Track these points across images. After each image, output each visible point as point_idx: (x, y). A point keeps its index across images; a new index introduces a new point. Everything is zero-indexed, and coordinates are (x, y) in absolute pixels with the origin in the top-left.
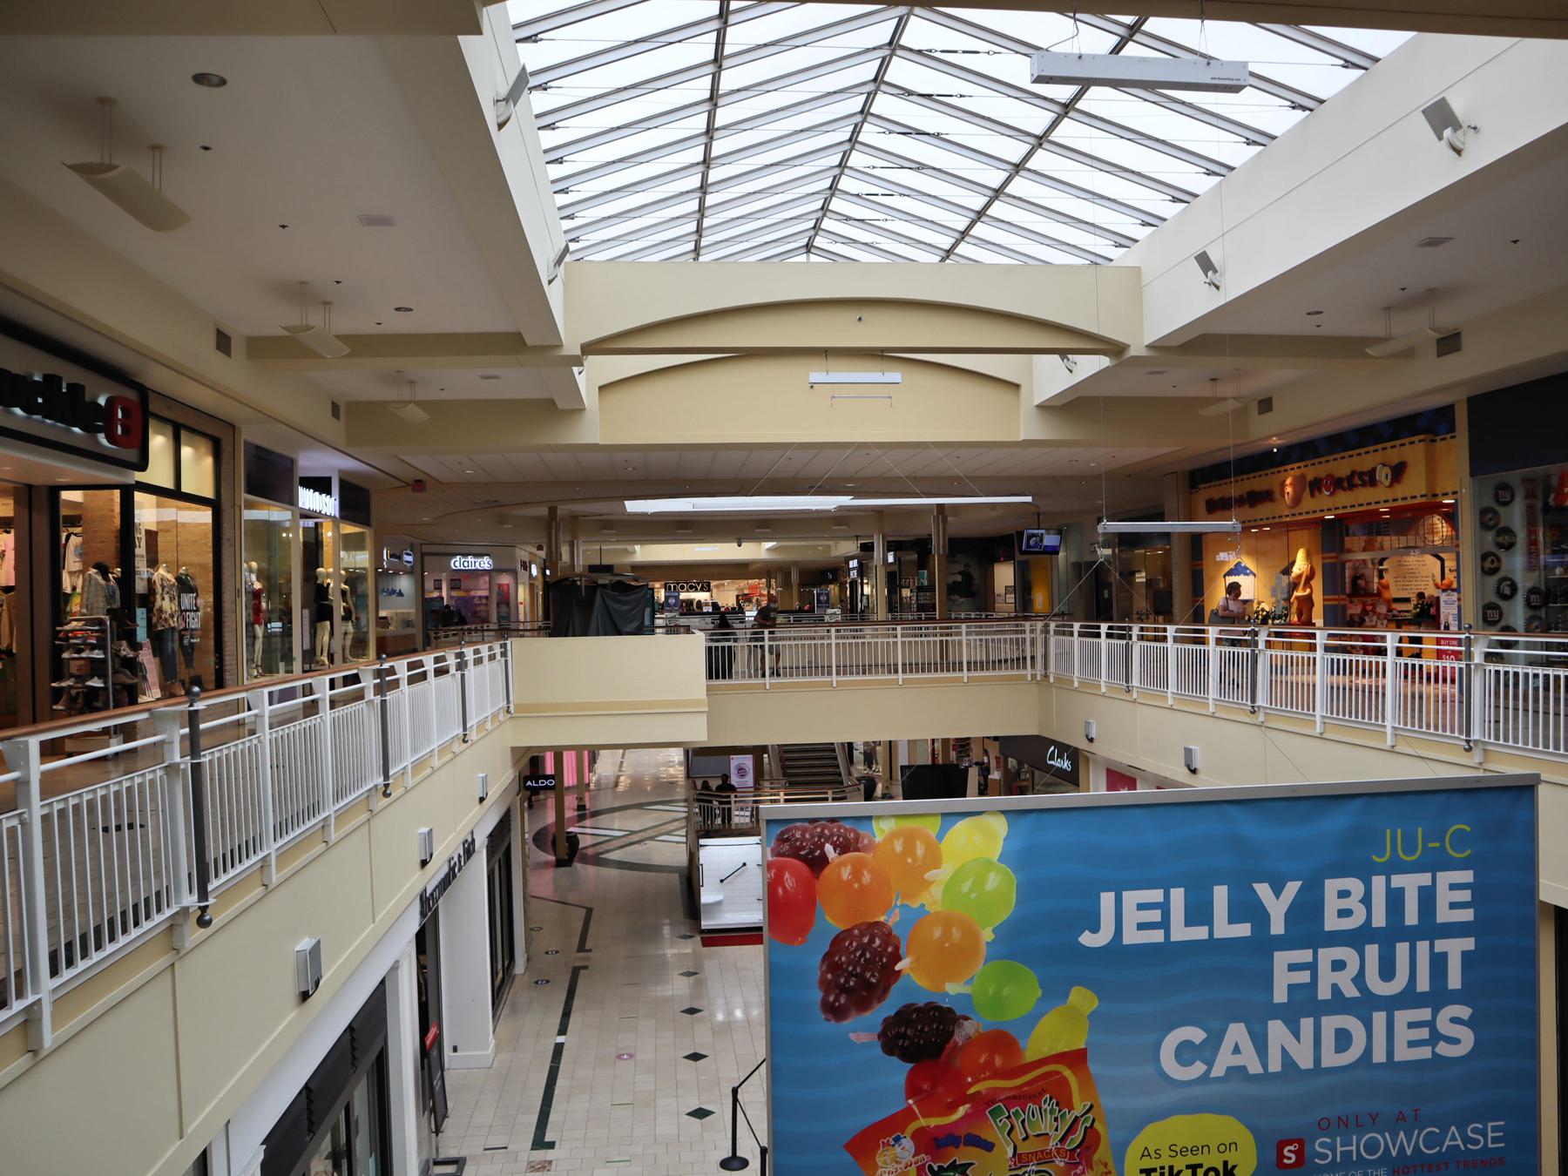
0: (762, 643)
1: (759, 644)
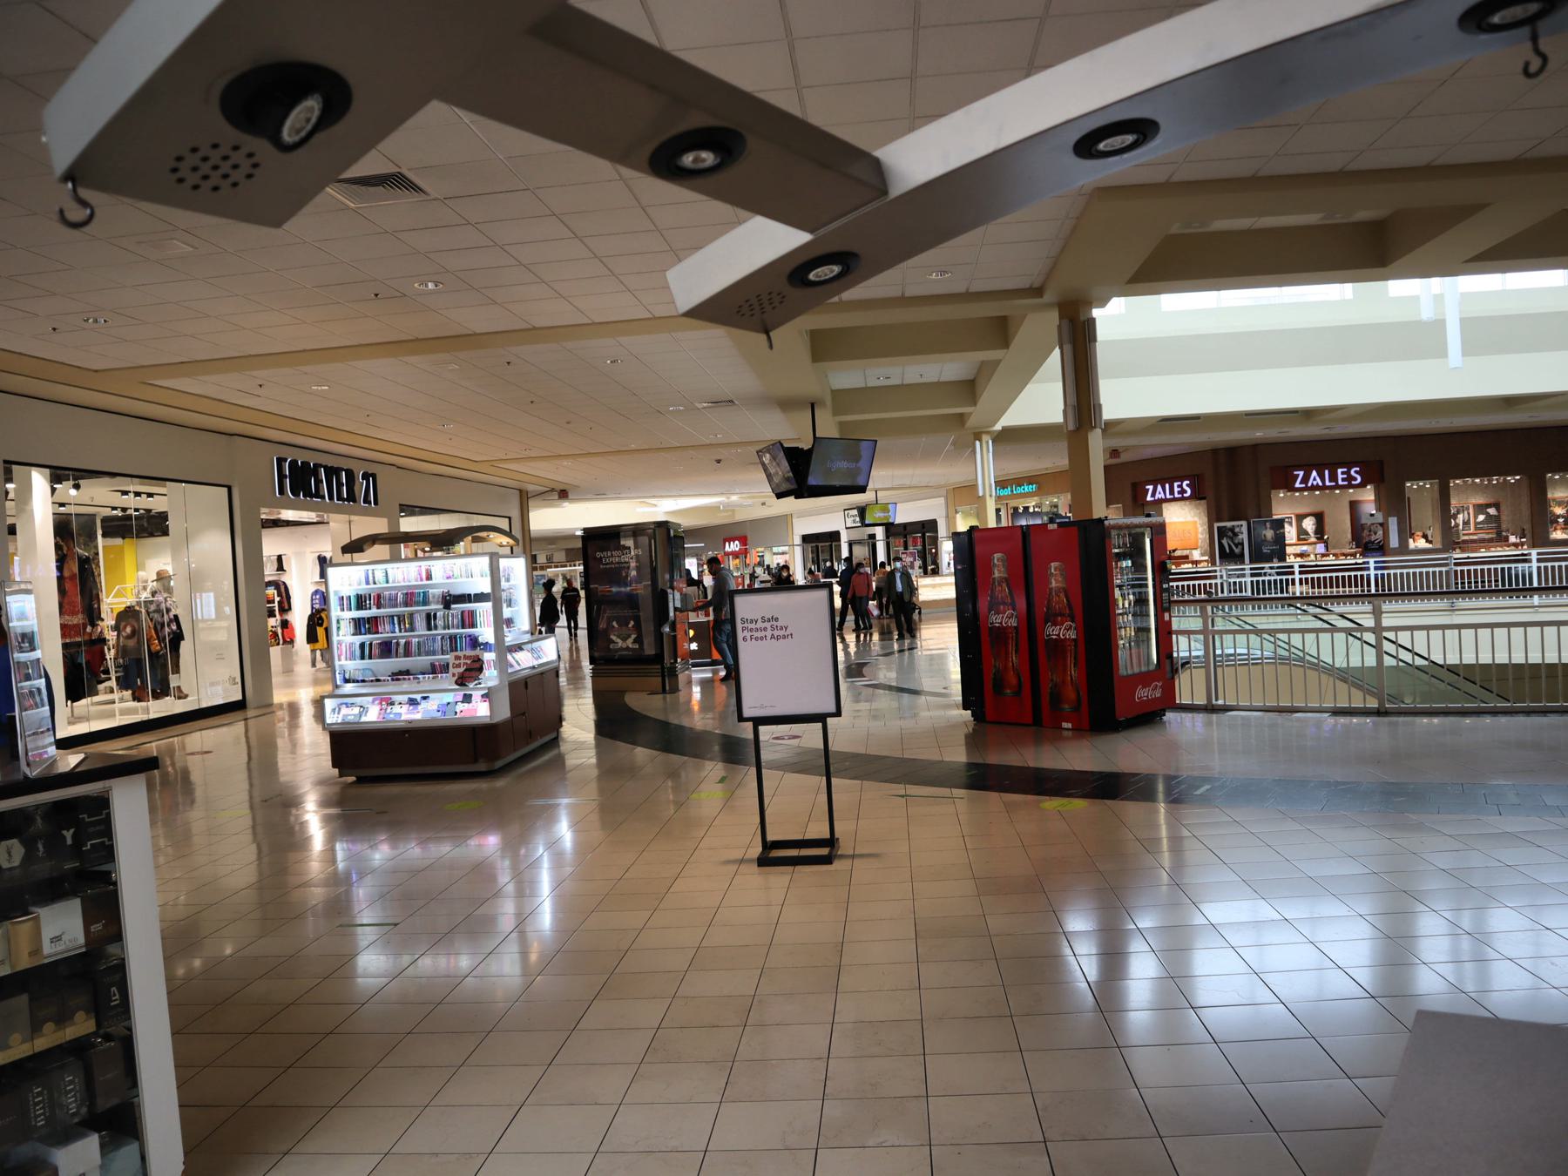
0: (1293, 577)
1: (1290, 577)
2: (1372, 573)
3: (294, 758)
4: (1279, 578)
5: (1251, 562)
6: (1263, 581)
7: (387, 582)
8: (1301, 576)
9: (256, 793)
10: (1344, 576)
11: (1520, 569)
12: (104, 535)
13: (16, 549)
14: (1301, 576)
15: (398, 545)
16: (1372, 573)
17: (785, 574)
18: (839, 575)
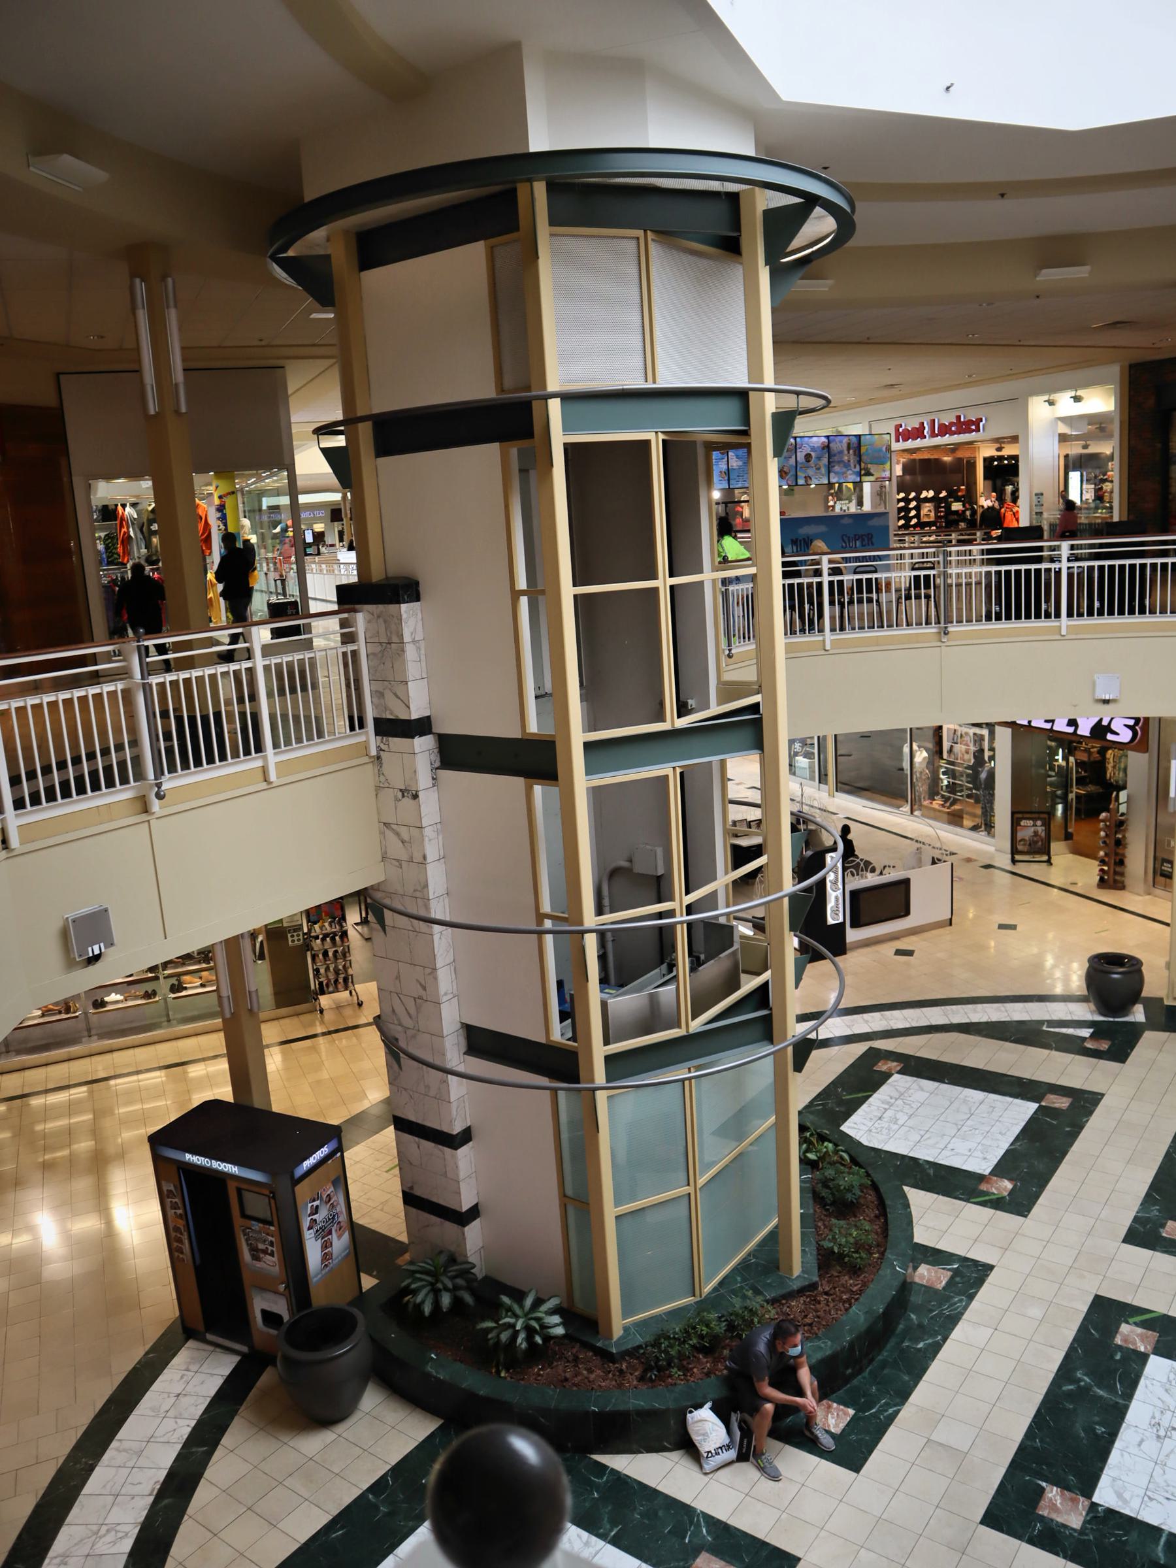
2: (826, 579)
3: (800, 541)
4: (994, 569)
5: (655, 578)
6: (800, 585)
7: (284, 594)
8: (831, 578)
9: (90, 683)
10: (1030, 570)
11: (1076, 571)
12: (716, 909)
13: (916, 816)
14: (831, 578)
15: (308, 295)
16: (1064, 565)
17: (821, 1272)
18: (500, 1322)
